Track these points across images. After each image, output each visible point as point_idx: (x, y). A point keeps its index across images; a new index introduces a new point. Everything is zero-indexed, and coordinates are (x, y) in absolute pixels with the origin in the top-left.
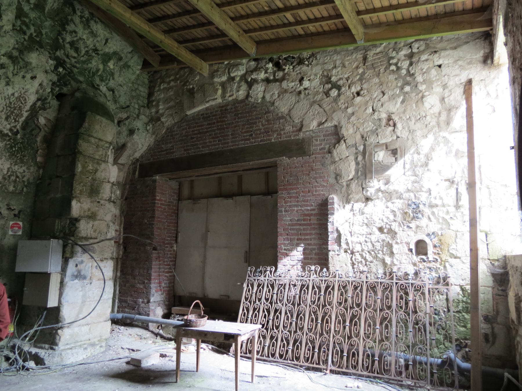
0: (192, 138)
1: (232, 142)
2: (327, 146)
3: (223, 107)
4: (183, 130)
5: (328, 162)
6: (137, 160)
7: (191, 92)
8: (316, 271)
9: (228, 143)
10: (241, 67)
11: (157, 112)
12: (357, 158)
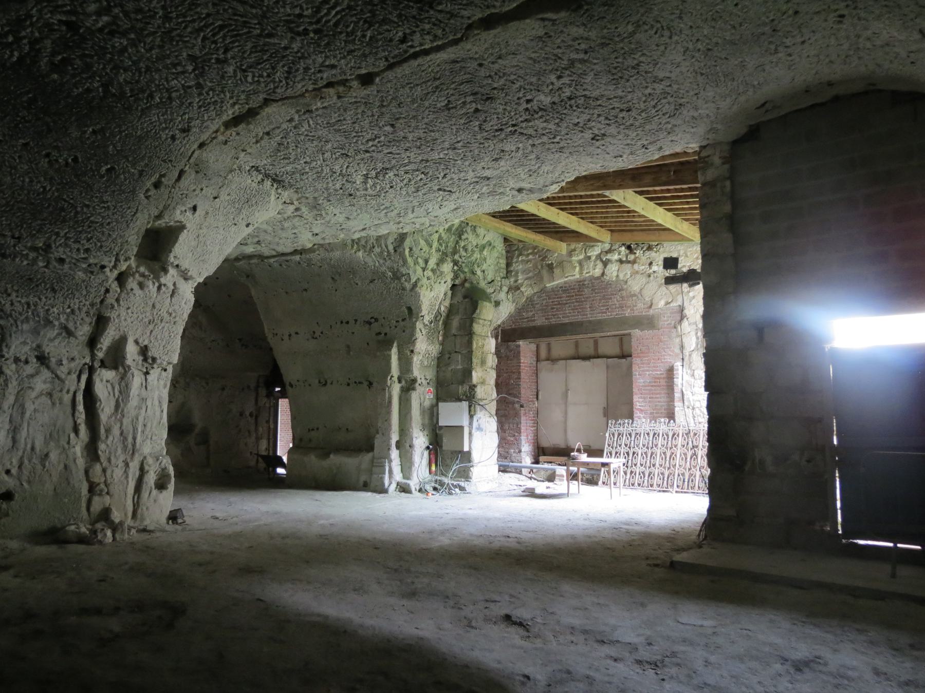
0: (553, 309)
1: (590, 314)
2: (673, 322)
3: (580, 282)
4: (543, 300)
5: (674, 334)
6: (499, 326)
7: (550, 267)
8: (665, 423)
9: (587, 315)
10: (596, 248)
11: (516, 281)
12: (697, 333)
